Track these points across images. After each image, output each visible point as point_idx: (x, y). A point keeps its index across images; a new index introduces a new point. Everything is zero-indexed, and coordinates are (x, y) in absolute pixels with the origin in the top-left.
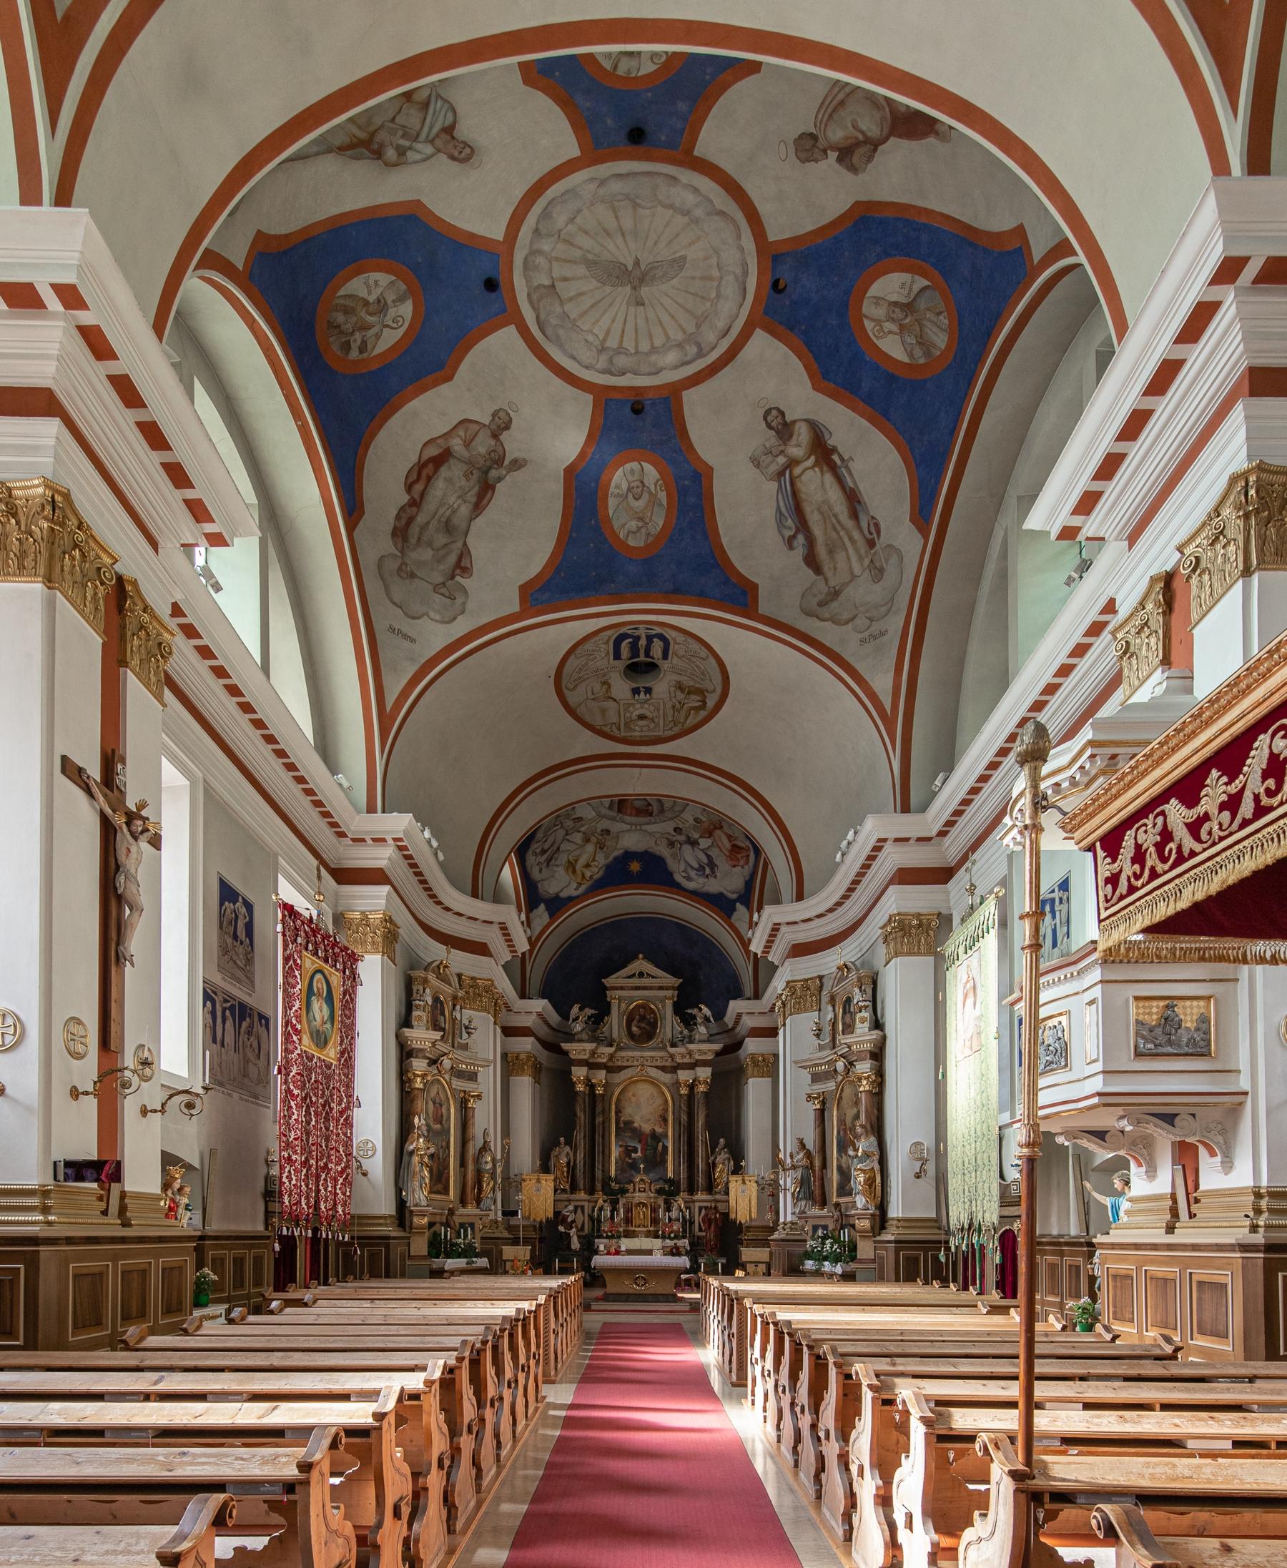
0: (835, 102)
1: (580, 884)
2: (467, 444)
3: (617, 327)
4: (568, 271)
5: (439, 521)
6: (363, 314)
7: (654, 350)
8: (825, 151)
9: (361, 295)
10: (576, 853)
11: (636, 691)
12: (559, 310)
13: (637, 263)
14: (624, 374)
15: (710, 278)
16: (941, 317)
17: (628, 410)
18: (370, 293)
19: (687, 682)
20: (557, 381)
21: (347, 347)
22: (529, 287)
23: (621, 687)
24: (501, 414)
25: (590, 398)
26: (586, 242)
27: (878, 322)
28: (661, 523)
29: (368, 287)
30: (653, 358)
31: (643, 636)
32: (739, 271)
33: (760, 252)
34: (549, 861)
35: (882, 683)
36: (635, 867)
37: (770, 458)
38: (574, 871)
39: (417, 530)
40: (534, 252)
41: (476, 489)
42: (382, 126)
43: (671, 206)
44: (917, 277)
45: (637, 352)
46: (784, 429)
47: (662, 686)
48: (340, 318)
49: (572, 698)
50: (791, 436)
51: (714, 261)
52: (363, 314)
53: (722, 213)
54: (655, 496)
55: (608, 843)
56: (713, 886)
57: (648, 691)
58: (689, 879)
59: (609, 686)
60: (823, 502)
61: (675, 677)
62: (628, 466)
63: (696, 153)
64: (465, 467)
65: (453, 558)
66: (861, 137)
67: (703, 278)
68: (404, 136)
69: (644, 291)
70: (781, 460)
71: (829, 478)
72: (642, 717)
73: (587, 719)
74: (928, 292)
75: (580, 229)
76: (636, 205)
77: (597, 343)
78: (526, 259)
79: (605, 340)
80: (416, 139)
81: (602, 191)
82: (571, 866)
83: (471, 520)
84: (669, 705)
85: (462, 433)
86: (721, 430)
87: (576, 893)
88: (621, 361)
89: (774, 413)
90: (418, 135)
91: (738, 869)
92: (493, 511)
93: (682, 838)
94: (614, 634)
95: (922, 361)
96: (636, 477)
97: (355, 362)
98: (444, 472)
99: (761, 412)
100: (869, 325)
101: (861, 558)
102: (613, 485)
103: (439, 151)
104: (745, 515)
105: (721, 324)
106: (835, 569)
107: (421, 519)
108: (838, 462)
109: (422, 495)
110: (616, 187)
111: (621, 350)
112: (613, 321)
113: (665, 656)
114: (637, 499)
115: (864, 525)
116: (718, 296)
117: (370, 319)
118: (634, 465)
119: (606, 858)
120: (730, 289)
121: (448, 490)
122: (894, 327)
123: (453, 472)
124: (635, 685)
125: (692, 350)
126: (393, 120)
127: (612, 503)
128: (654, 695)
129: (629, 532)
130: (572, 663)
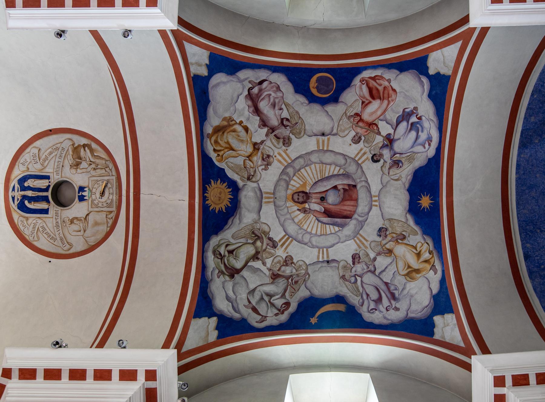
1: (433, 267)
10: (401, 265)
11: (82, 199)
19: (69, 160)
23: (78, 209)
34: (393, 297)
36: (425, 202)
38: (418, 271)
47: (78, 179)
49: (79, 247)
55: (399, 230)
56: (426, 109)
57: (82, 189)
58: (429, 140)
59: (76, 218)
61: (67, 168)
73: (100, 237)
82: (412, 273)
84: (93, 173)
87: (440, 273)
91: (394, 85)
93: (386, 153)
94: (17, 215)
113: (48, 177)
119: (416, 234)
124: (77, 199)
130: (43, 243)
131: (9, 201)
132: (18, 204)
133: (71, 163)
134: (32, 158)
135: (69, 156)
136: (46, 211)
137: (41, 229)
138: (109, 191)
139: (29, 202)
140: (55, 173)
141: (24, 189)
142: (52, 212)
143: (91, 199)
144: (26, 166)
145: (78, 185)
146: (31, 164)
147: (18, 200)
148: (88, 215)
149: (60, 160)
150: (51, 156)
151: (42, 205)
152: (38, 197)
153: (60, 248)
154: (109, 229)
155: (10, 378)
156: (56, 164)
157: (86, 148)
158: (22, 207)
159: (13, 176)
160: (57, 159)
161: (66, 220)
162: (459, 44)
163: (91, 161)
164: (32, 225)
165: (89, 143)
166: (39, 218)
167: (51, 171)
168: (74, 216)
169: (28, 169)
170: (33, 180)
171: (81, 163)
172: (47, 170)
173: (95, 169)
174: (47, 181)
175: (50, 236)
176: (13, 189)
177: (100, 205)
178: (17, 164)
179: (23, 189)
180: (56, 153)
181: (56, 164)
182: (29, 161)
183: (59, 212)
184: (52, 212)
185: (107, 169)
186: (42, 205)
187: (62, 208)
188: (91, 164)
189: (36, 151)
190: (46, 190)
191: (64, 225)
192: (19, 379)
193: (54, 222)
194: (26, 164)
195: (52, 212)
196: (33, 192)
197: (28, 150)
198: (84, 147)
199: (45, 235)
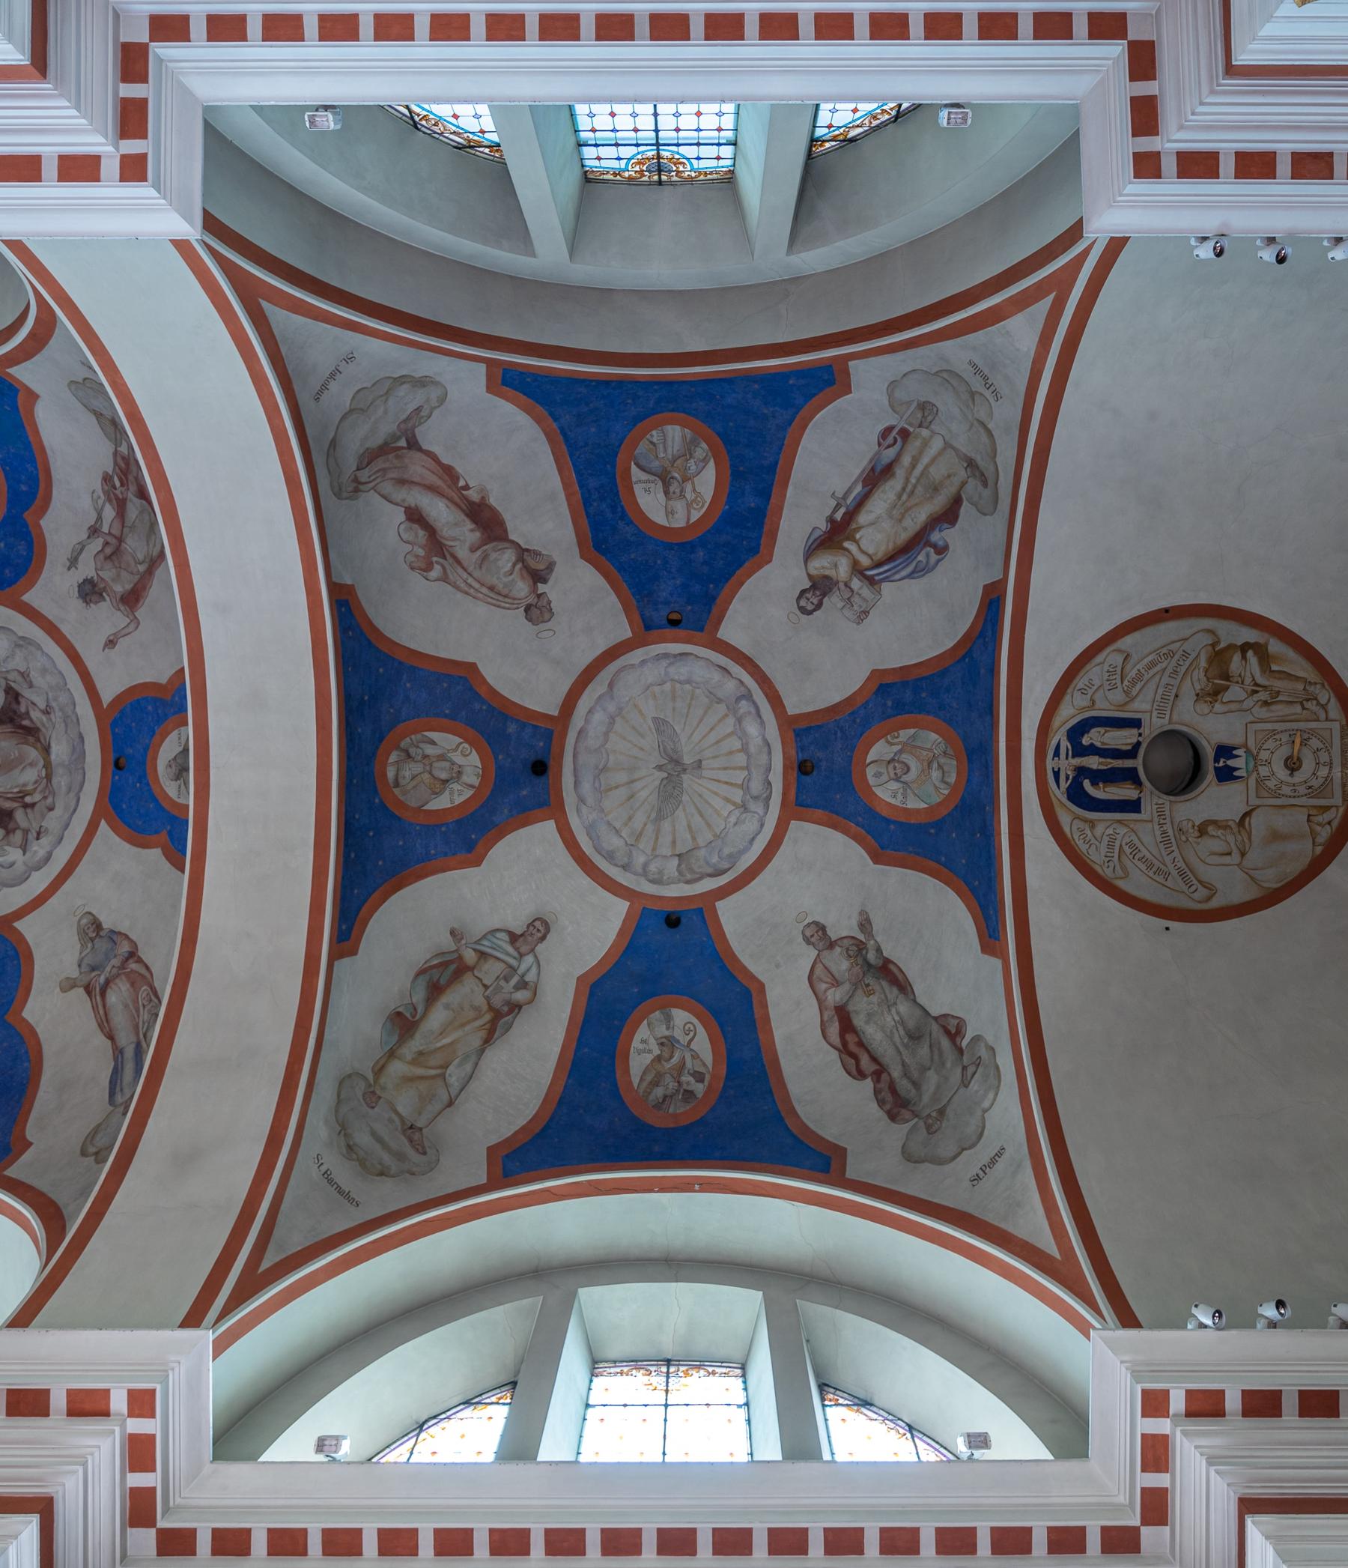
0: (492, 595)
2: (836, 983)
3: (723, 790)
4: (666, 840)
5: (906, 1046)
6: (667, 1065)
7: (744, 749)
8: (539, 596)
9: (648, 1062)
11: (1226, 775)
12: (702, 852)
13: (659, 768)
14: (769, 784)
15: (673, 691)
16: (655, 440)
17: (807, 779)
18: (650, 1051)
19: (1198, 680)
20: (776, 861)
21: (689, 1094)
22: (679, 881)
23: (1215, 800)
24: (808, 934)
26: (639, 819)
27: (689, 506)
28: (934, 736)
29: (644, 1051)
30: (752, 749)
31: (1078, 761)
32: (664, 663)
33: (644, 643)
35: (1022, 332)
37: (856, 599)
39: (905, 1082)
40: (645, 873)
41: (884, 984)
42: (487, 998)
43: (606, 734)
44: (634, 479)
45: (747, 768)
46: (820, 587)
47: (1214, 727)
48: (659, 1092)
49: (1235, 890)
50: (826, 577)
51: (657, 689)
52: (667, 1065)
53: (611, 685)
54: (905, 744)
57: (1224, 751)
59: (1214, 822)
60: (891, 517)
61: (1187, 702)
62: (871, 780)
63: (556, 714)
64: (860, 992)
65: (945, 1043)
66: (519, 566)
67: (674, 698)
68: (507, 979)
69: (687, 760)
70: (856, 584)
71: (863, 518)
72: (1293, 765)
74: (643, 462)
75: (626, 824)
76: (604, 769)
77: (737, 812)
78: (651, 881)
79: (734, 804)
80: (514, 970)
81: (590, 801)
83: (915, 1001)
84: (1262, 713)
85: (824, 986)
86: (829, 662)
88: (756, 786)
89: (803, 603)
90: (511, 967)
92: (912, 969)
94: (1068, 815)
95: (704, 445)
96: (883, 770)
97: (706, 1093)
98: (858, 1021)
99: (804, 618)
100: (695, 516)
101: (926, 444)
102: (892, 801)
103: (533, 950)
104: (914, 623)
105: (716, 676)
106: (949, 476)
107: (896, 1073)
108: (842, 511)
109: (874, 1059)
110: (586, 787)
111: (745, 786)
112: (716, 794)
114: (909, 769)
115: (891, 453)
116: (688, 682)
117: (675, 1059)
118: (870, 772)
120: (681, 671)
121: (880, 1025)
122: (688, 487)
123: (861, 1008)
125: (744, 706)
126: (486, 987)
127: (913, 804)
128: (1237, 740)
129: (943, 781)
130: (1138, 884)
133: (1198, 687)
136: (1134, 806)
137: (1126, 848)
139: (1094, 784)
140: (1155, 713)
143: (1255, 775)
145: (1213, 742)
146: (1101, 691)
147: (1067, 778)
148: (1248, 814)
150: (1151, 672)
151: (1124, 792)
152: (1113, 770)
154: (1319, 849)
156: (1160, 691)
157: (1250, 654)
158: (1077, 795)
159: (1057, 721)
160: (1165, 680)
162: (1045, 304)
163: (1256, 685)
164: (1106, 839)
165: (1262, 641)
167: (1146, 707)
169: (1093, 702)
170: (1102, 730)
171: (1227, 688)
172: (1136, 705)
173: (1266, 703)
174: (1135, 731)
176: (1057, 754)
178: (1069, 691)
179: (1079, 750)
180: (1164, 665)
181: (1160, 691)
182: (1097, 682)
185: (1311, 705)
186: (1124, 792)
187: (1172, 798)
188: (1257, 692)
189: (1119, 659)
190: (1132, 753)
191: (1184, 838)
193: (1158, 833)
194: (1090, 692)
196: (1102, 760)
197: (1099, 658)
199: (1139, 864)
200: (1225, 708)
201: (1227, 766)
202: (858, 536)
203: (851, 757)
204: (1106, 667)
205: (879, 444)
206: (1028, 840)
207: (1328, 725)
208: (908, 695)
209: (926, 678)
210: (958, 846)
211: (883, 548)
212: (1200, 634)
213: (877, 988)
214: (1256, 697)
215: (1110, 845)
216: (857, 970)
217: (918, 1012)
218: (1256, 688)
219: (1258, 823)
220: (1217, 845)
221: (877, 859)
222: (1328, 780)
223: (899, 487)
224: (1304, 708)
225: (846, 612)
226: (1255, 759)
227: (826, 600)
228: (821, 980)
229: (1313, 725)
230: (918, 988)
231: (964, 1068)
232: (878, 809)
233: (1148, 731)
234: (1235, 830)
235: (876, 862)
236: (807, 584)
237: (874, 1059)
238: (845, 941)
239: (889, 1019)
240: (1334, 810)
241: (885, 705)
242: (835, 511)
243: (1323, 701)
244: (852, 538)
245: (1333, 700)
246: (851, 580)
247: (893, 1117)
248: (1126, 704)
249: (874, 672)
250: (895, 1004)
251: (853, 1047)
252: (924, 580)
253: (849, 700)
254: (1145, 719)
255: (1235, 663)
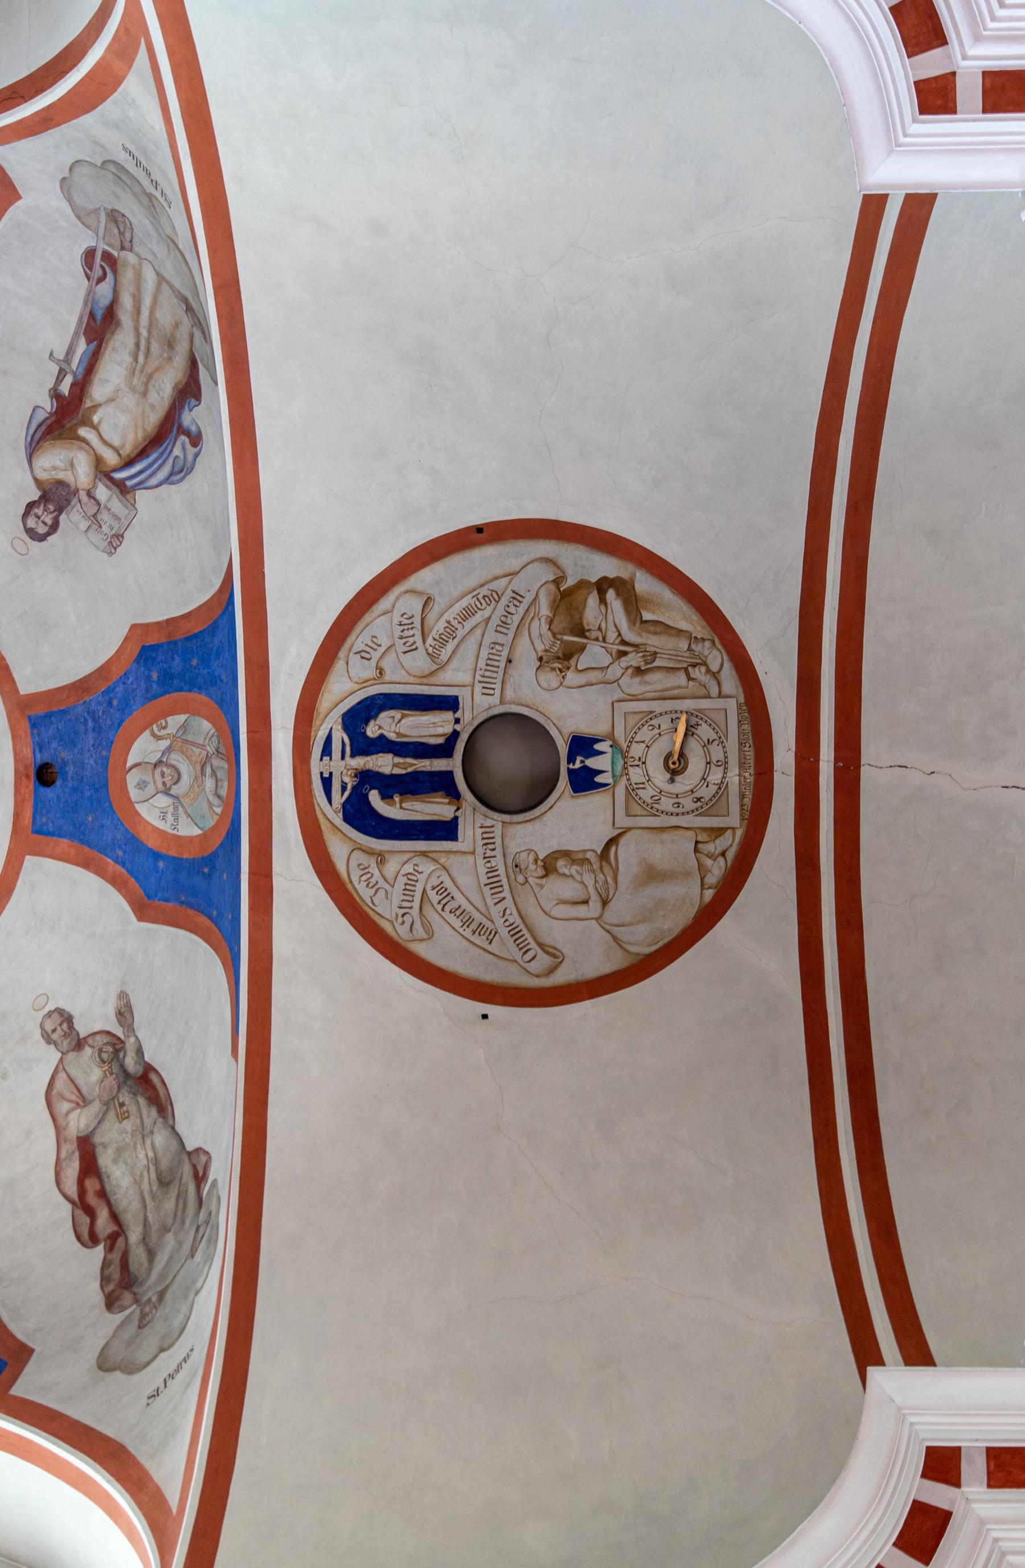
2: (83, 1101)
11: (584, 782)
17: (49, 793)
19: (538, 637)
23: (571, 821)
24: (49, 1027)
25: (29, 859)
31: (360, 762)
37: (104, 516)
41: (142, 1101)
47: (568, 708)
49: (590, 957)
50: (61, 483)
54: (174, 738)
57: (582, 745)
59: (566, 854)
60: (133, 389)
61: (525, 670)
62: (134, 794)
64: (112, 1114)
70: (102, 492)
71: (98, 392)
73: (673, 923)
83: (173, 1128)
84: (632, 685)
85: (65, 1106)
89: (31, 523)
94: (343, 844)
96: (148, 778)
98: (105, 1160)
108: (68, 380)
109: (114, 1217)
113: (450, 704)
118: (132, 779)
123: (112, 1136)
127: (188, 830)
130: (447, 949)
131: (310, 792)
132: (344, 805)
133: (540, 647)
134: (397, 633)
135: (535, 624)
136: (447, 830)
137: (432, 895)
138: (707, 753)
139: (386, 796)
140: (478, 688)
141: (363, 746)
142: (469, 832)
143: (623, 782)
144: (373, 662)
146: (392, 655)
147: (344, 788)
148: (613, 841)
149: (500, 638)
151: (433, 808)
152: (415, 776)
153: (513, 968)
154: (709, 894)
155: (955, 1482)
156: (484, 653)
157: (611, 594)
158: (359, 815)
159: (324, 702)
160: (490, 636)
161: (526, 860)
163: (624, 642)
164: (402, 880)
165: (625, 575)
166: (424, 854)
167: (465, 678)
168: (553, 845)
169: (381, 672)
170: (397, 714)
171: (582, 648)
172: (448, 675)
173: (638, 671)
174: (449, 716)
175: (471, 920)
176: (327, 750)
177: (666, 804)
178: (342, 654)
179: (362, 746)
180: (486, 613)
182: (385, 641)
183: (498, 830)
184: (469, 833)
185: (697, 673)
186: (433, 808)
187: (506, 818)
188: (624, 654)
189: (414, 606)
190: (445, 750)
191: (521, 878)
192: (989, 1486)
193: (482, 870)
194: (376, 656)
195: (469, 833)
196: (398, 760)
197: (385, 604)
198: (601, 585)
199: (451, 919)
200: (581, 679)
201: (585, 768)
202: (96, 419)
203: (107, 758)
204: (397, 619)
205: (88, 278)
206: (279, 883)
207: (720, 703)
208: (177, 664)
209: (195, 636)
210: (197, 889)
211: (131, 437)
212: (536, 565)
213: (133, 1109)
214: (624, 662)
215: (408, 890)
216: (111, 1081)
217: (174, 1145)
218: (624, 648)
219: (629, 855)
220: (568, 889)
221: (143, 911)
222: (722, 787)
223: (131, 342)
224: (690, 679)
225: (92, 535)
226: (624, 757)
227: (63, 518)
228: (62, 1097)
229: (704, 704)
230: (180, 1108)
231: (198, 1227)
232: (143, 837)
233: (470, 716)
234: (596, 866)
235: (140, 919)
236: (35, 495)
237: (114, 1217)
238: (98, 1037)
239: (141, 1155)
240: (729, 832)
241: (148, 678)
242: (59, 379)
243: (715, 668)
244: (87, 422)
245: (727, 665)
246: (95, 487)
247: (111, 1303)
248: (432, 674)
249: (134, 627)
250: (152, 1132)
251: (92, 1199)
252: (184, 485)
253: (102, 672)
254: (464, 696)
255: (591, 610)
